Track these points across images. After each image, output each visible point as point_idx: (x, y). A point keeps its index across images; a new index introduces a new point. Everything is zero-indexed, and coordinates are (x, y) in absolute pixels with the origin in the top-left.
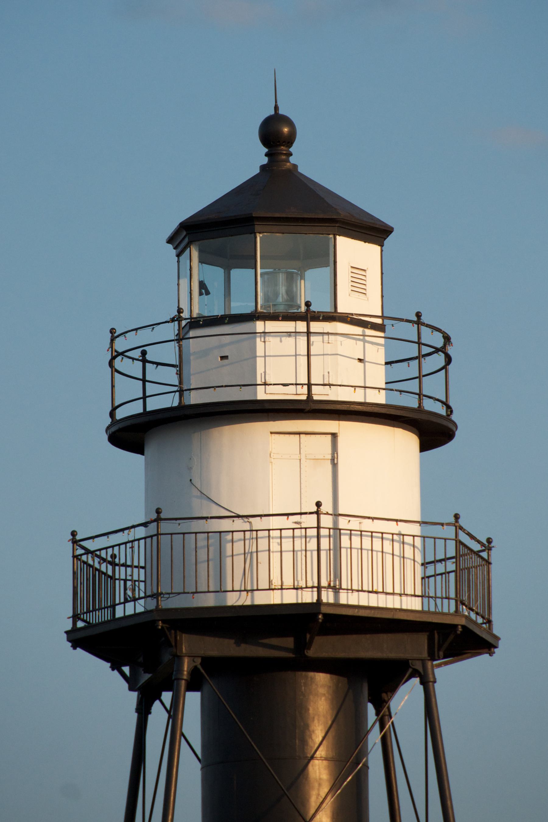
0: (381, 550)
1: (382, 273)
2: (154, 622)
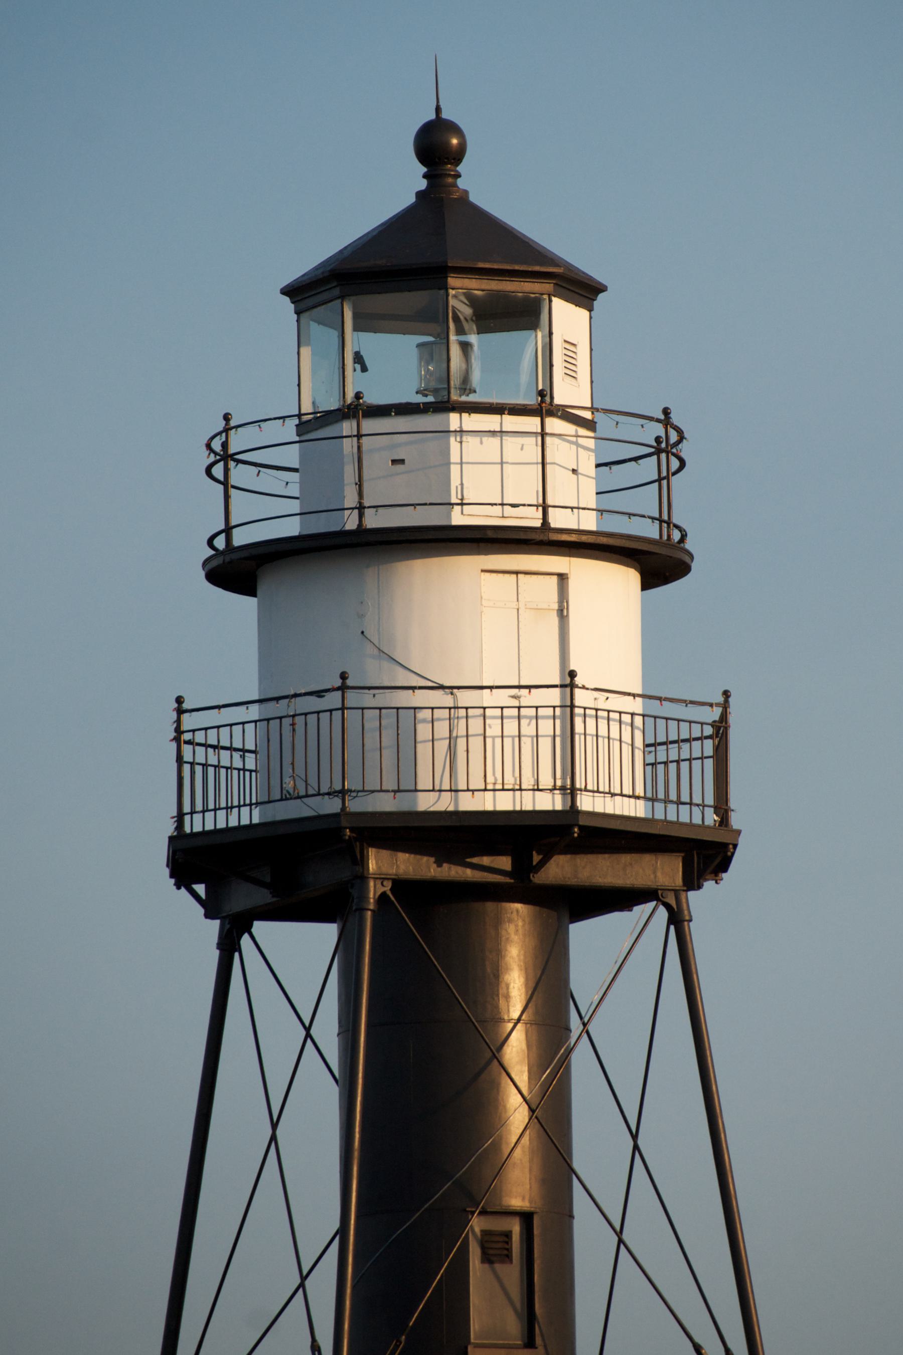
0: (618, 738)
1: (591, 350)
2: (340, 830)
